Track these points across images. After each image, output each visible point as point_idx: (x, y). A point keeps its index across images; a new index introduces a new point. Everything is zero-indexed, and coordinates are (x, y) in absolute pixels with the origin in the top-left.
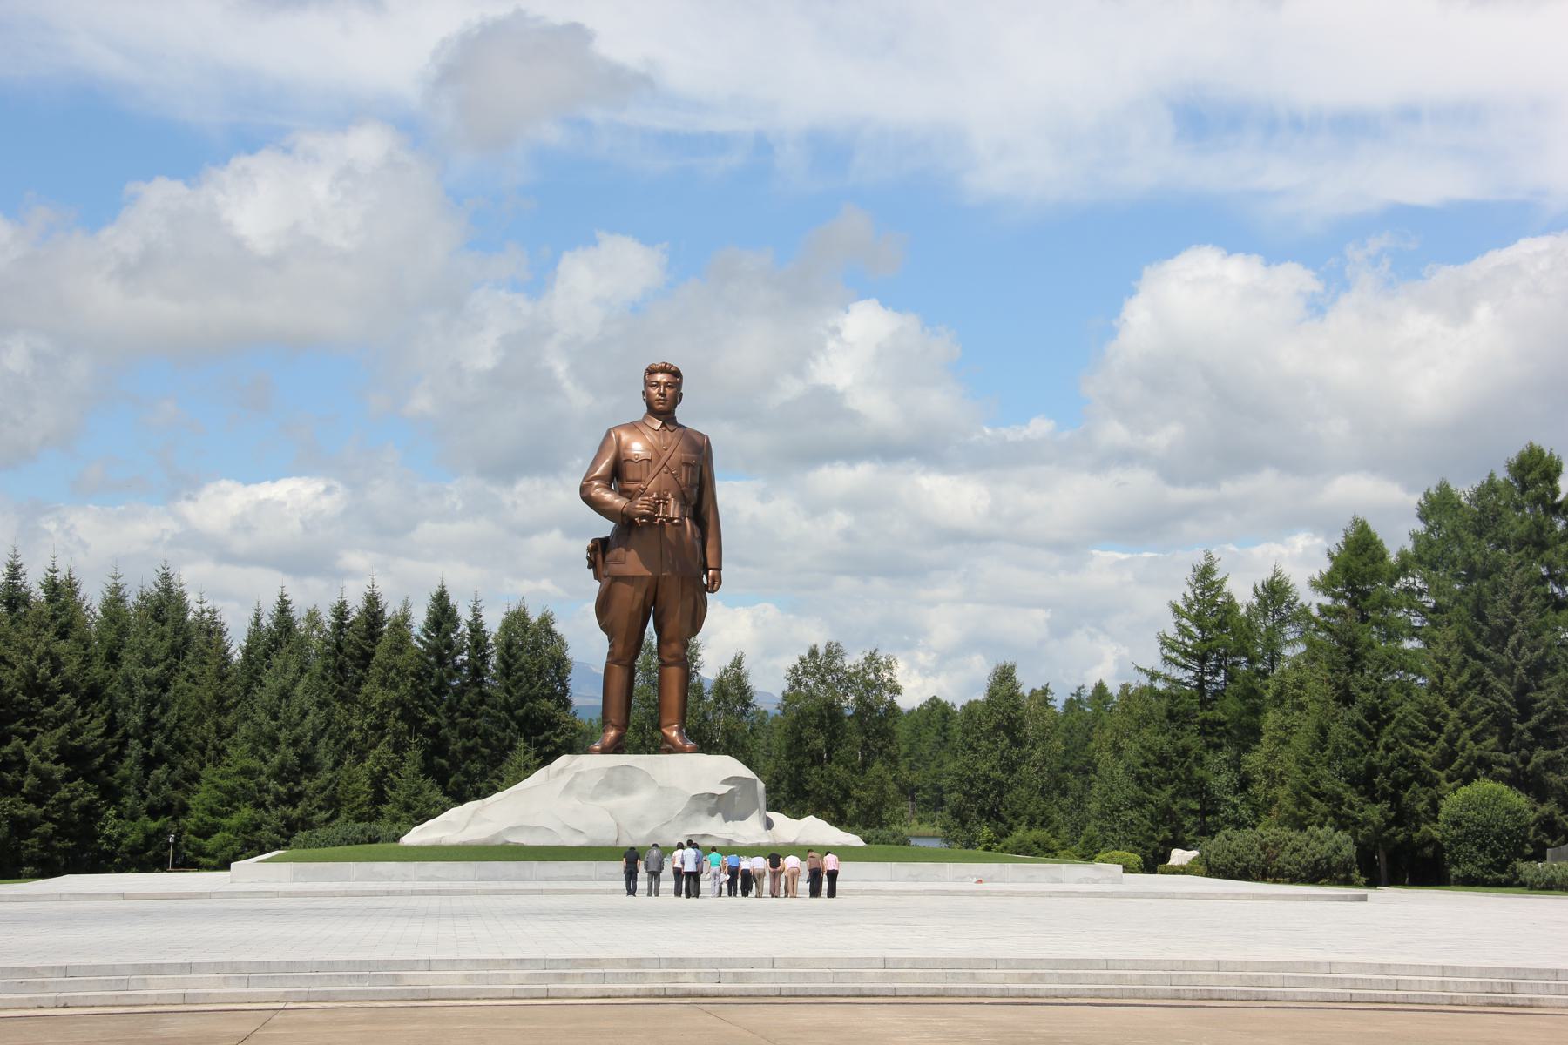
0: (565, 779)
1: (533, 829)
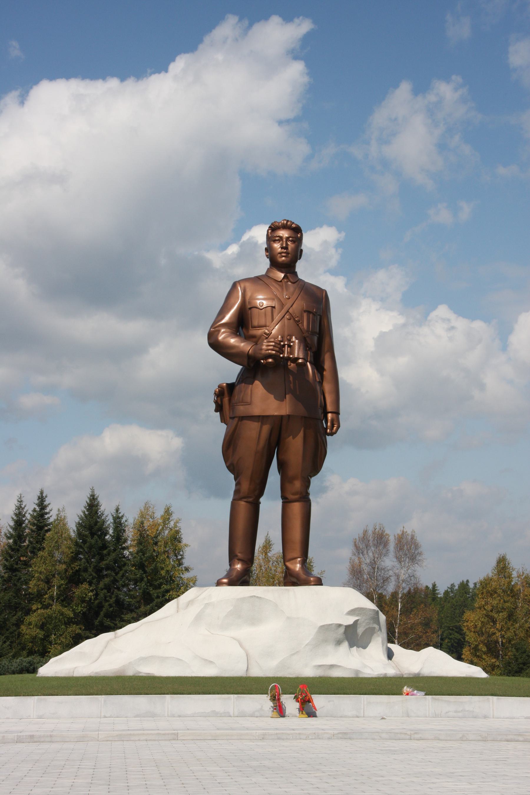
0: (194, 610)
1: (163, 659)
